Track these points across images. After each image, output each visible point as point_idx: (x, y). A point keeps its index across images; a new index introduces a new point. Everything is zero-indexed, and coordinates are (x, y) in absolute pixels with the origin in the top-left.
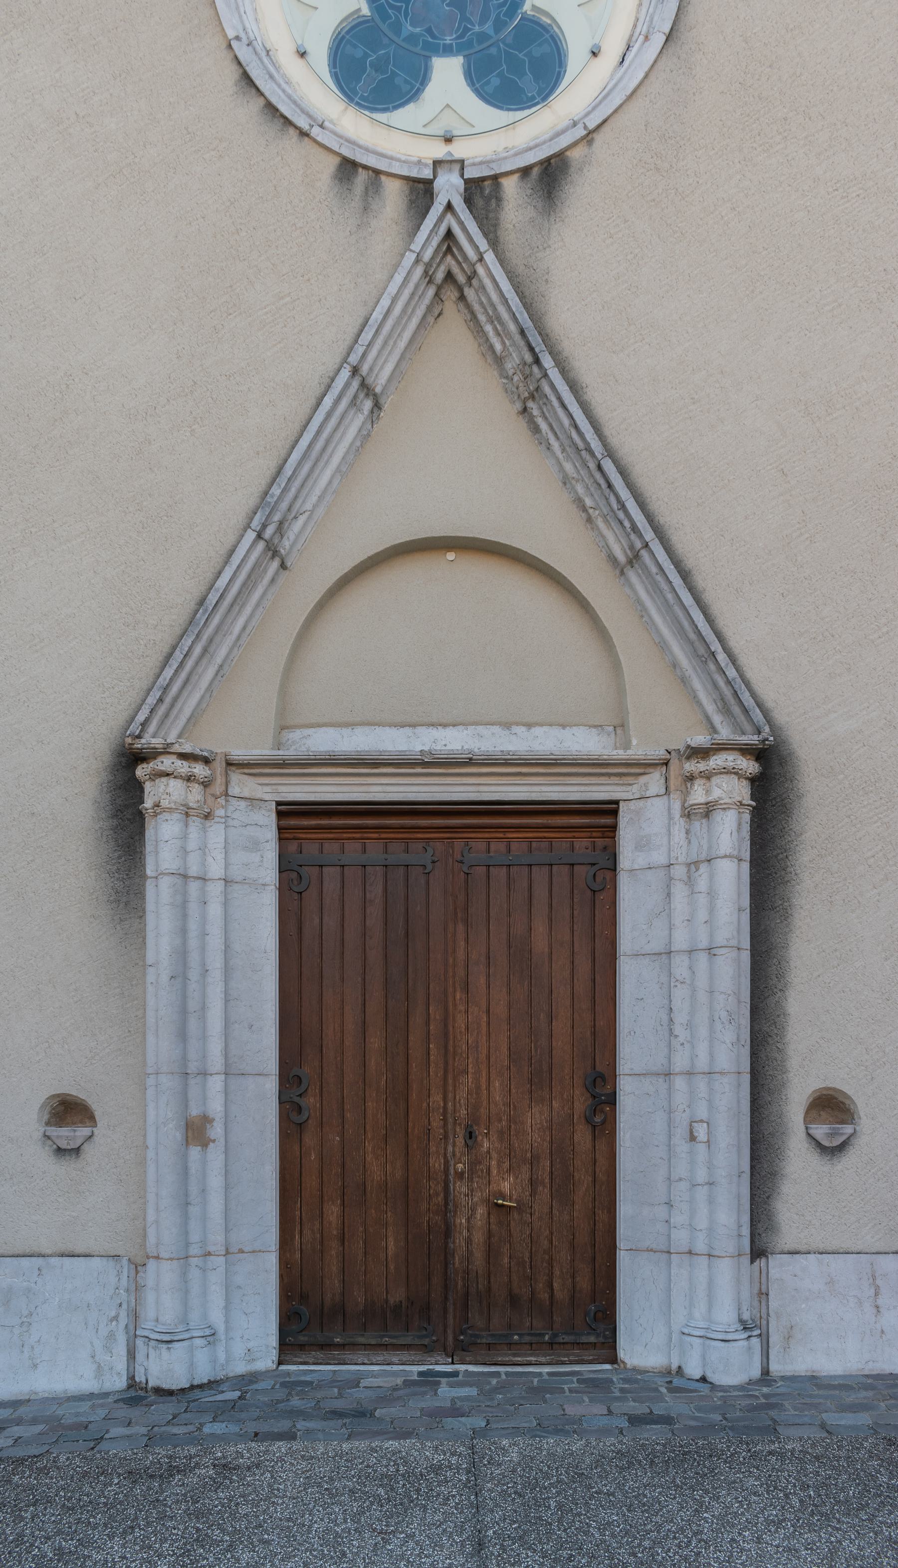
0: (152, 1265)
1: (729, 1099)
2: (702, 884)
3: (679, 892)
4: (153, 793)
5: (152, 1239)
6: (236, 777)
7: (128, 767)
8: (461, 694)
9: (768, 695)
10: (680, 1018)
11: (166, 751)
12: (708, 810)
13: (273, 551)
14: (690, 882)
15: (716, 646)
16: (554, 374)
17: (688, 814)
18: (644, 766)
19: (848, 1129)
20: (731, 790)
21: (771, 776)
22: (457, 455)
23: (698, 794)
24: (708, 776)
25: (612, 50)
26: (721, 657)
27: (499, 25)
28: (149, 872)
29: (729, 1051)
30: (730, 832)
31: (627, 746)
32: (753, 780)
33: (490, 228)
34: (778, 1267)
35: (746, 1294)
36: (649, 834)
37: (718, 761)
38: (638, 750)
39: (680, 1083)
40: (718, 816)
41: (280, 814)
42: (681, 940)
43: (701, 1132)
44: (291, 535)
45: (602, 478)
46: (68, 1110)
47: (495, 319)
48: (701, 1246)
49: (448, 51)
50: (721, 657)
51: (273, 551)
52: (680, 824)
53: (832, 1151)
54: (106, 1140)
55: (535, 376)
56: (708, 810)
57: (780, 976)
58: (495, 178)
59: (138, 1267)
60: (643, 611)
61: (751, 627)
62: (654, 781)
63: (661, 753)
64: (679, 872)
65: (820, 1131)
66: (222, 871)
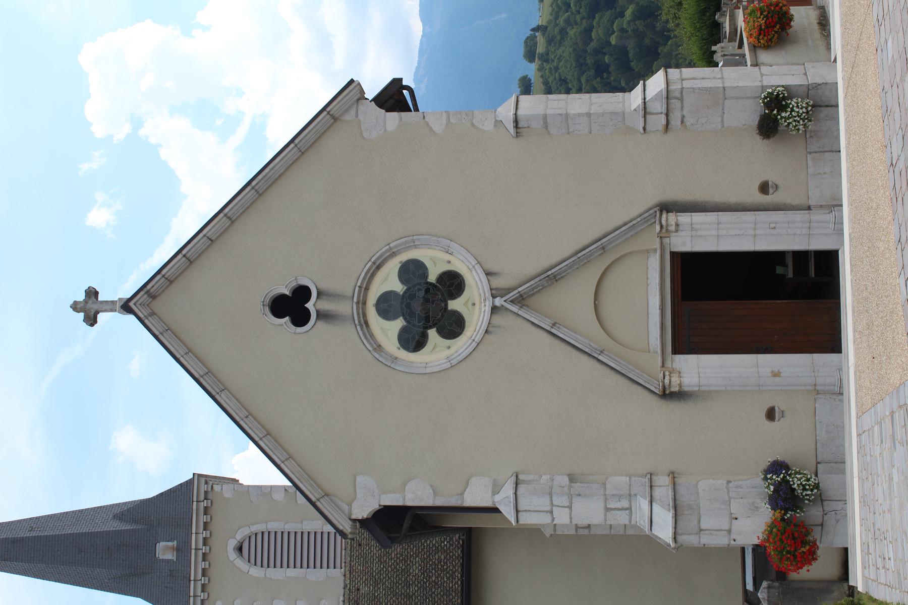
0: (818, 388)
1: (762, 216)
2: (698, 226)
3: (699, 233)
4: (675, 389)
5: (809, 388)
6: (666, 365)
7: (667, 395)
8: (645, 298)
9: (642, 209)
10: (738, 232)
11: (663, 382)
12: (677, 225)
13: (602, 352)
14: (697, 230)
15: (631, 224)
16: (553, 271)
17: (677, 231)
18: (662, 243)
19: (770, 183)
20: (672, 218)
21: (666, 207)
22: (573, 301)
23: (673, 228)
24: (667, 225)
25: (448, 257)
26: (634, 222)
27: (439, 290)
28: (697, 389)
29: (749, 217)
30: (684, 218)
31: (655, 250)
32: (668, 212)
33: (509, 290)
34: (812, 203)
35: (821, 211)
36: (684, 243)
37: (664, 223)
38: (657, 245)
39: (758, 232)
40: (679, 222)
41: (675, 354)
42: (714, 232)
43: (772, 225)
44: (596, 347)
45: (580, 258)
46: (771, 415)
47: (533, 289)
48: (808, 225)
49: (446, 305)
50: (634, 222)
51: (602, 352)
52: (679, 233)
53: (777, 187)
54: (779, 405)
55: (551, 278)
56: (677, 225)
57: (725, 203)
58: (491, 289)
59: (818, 393)
60: (617, 245)
61: (621, 215)
62: (666, 241)
63: (658, 239)
64: (694, 233)
65: (771, 191)
66: (696, 369)
